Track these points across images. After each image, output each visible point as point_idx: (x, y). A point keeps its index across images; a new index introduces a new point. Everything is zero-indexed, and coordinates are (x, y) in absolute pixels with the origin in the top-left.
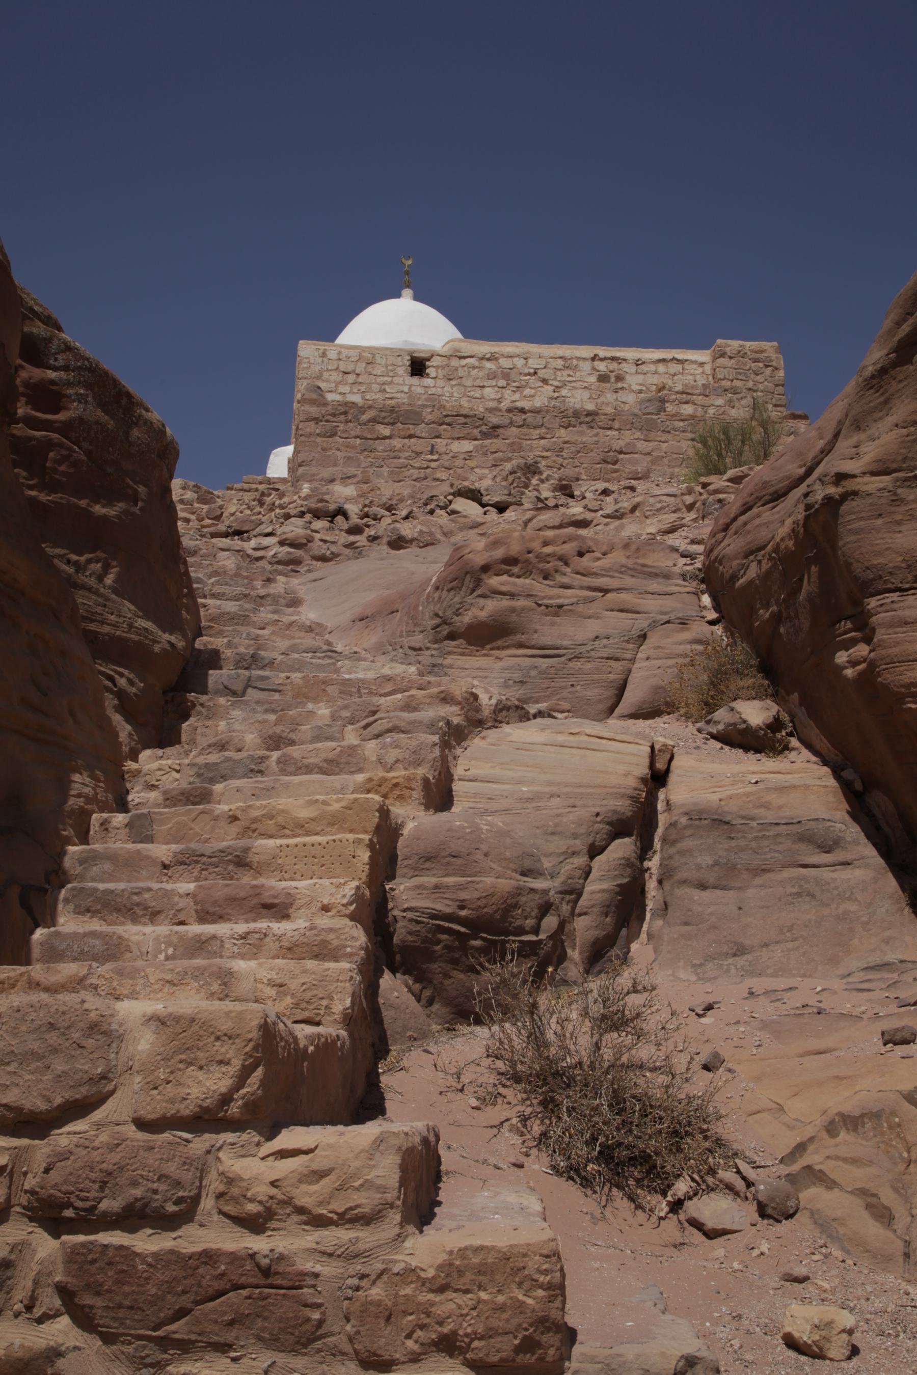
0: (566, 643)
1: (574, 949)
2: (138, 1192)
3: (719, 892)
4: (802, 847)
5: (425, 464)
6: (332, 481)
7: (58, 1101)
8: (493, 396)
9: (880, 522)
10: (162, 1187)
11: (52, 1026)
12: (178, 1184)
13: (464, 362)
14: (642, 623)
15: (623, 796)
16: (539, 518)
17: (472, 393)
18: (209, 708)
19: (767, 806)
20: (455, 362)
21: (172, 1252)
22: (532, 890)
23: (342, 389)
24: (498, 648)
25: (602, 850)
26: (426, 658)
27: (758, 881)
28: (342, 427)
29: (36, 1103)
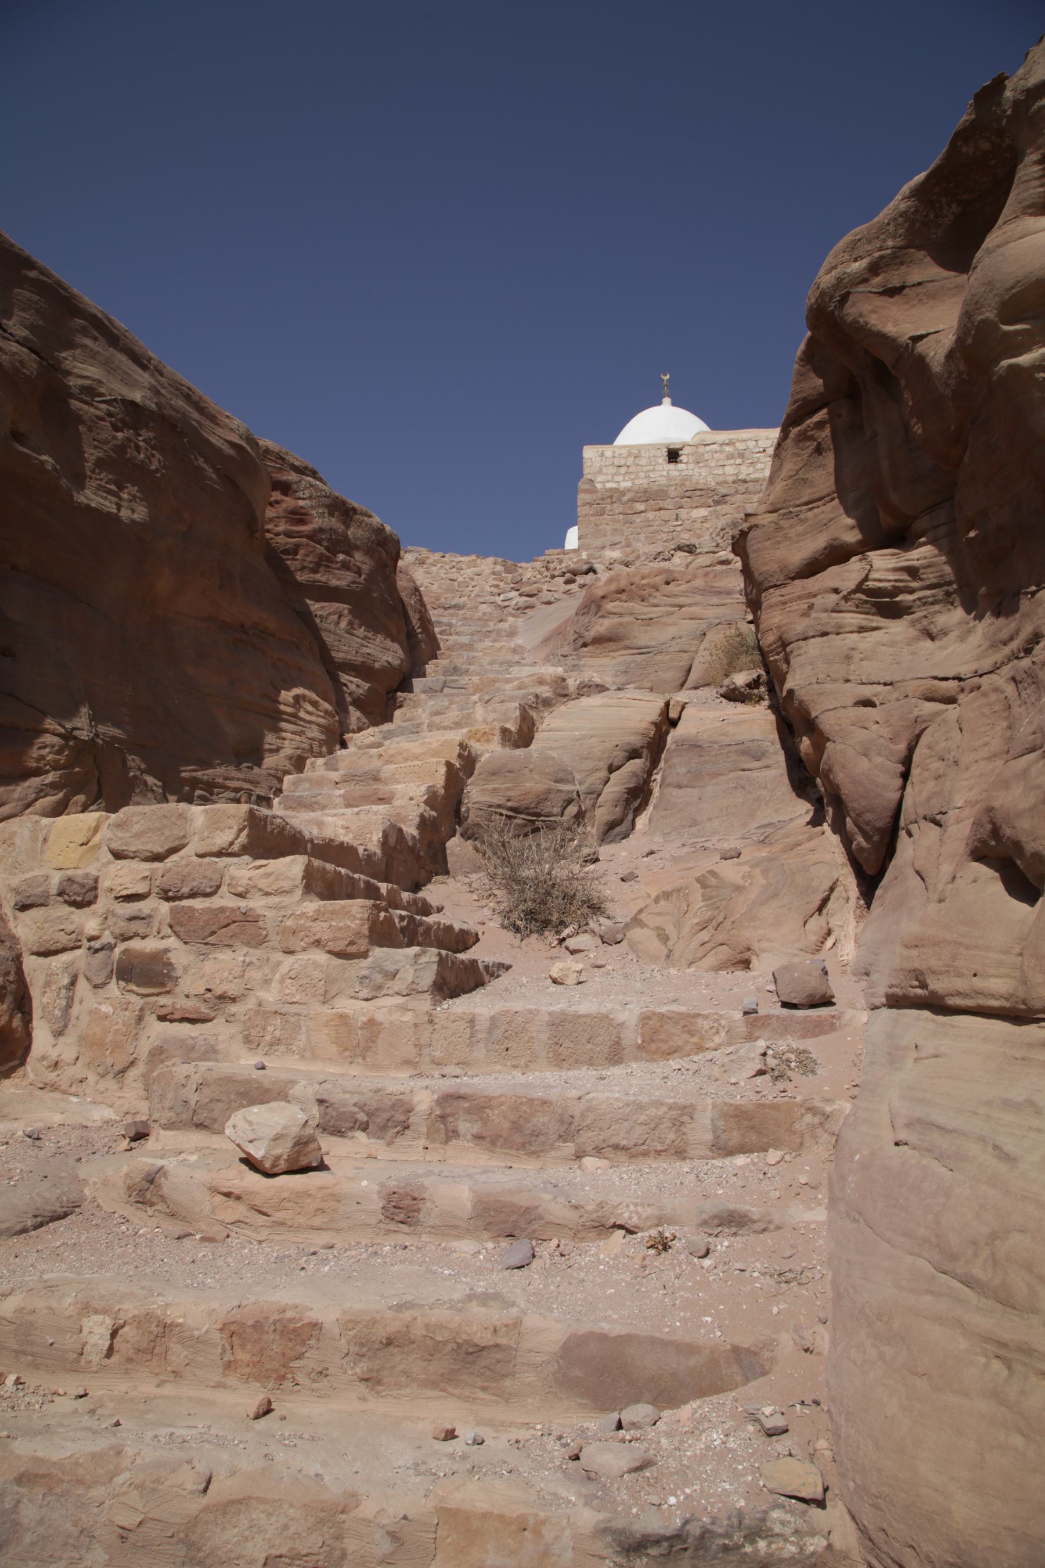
0: (653, 643)
1: (593, 827)
2: (195, 884)
3: (689, 790)
4: (744, 758)
5: (672, 529)
6: (604, 548)
7: (166, 848)
8: (732, 472)
9: (768, 543)
10: (205, 881)
11: (165, 816)
12: (211, 880)
13: (708, 448)
14: (703, 625)
15: (636, 734)
16: (698, 561)
17: (716, 472)
18: (415, 701)
19: (726, 734)
20: (701, 449)
21: (209, 908)
22: (559, 791)
23: (617, 479)
24: (613, 651)
25: (619, 768)
26: (570, 661)
27: (714, 781)
28: (609, 507)
29: (159, 849)
